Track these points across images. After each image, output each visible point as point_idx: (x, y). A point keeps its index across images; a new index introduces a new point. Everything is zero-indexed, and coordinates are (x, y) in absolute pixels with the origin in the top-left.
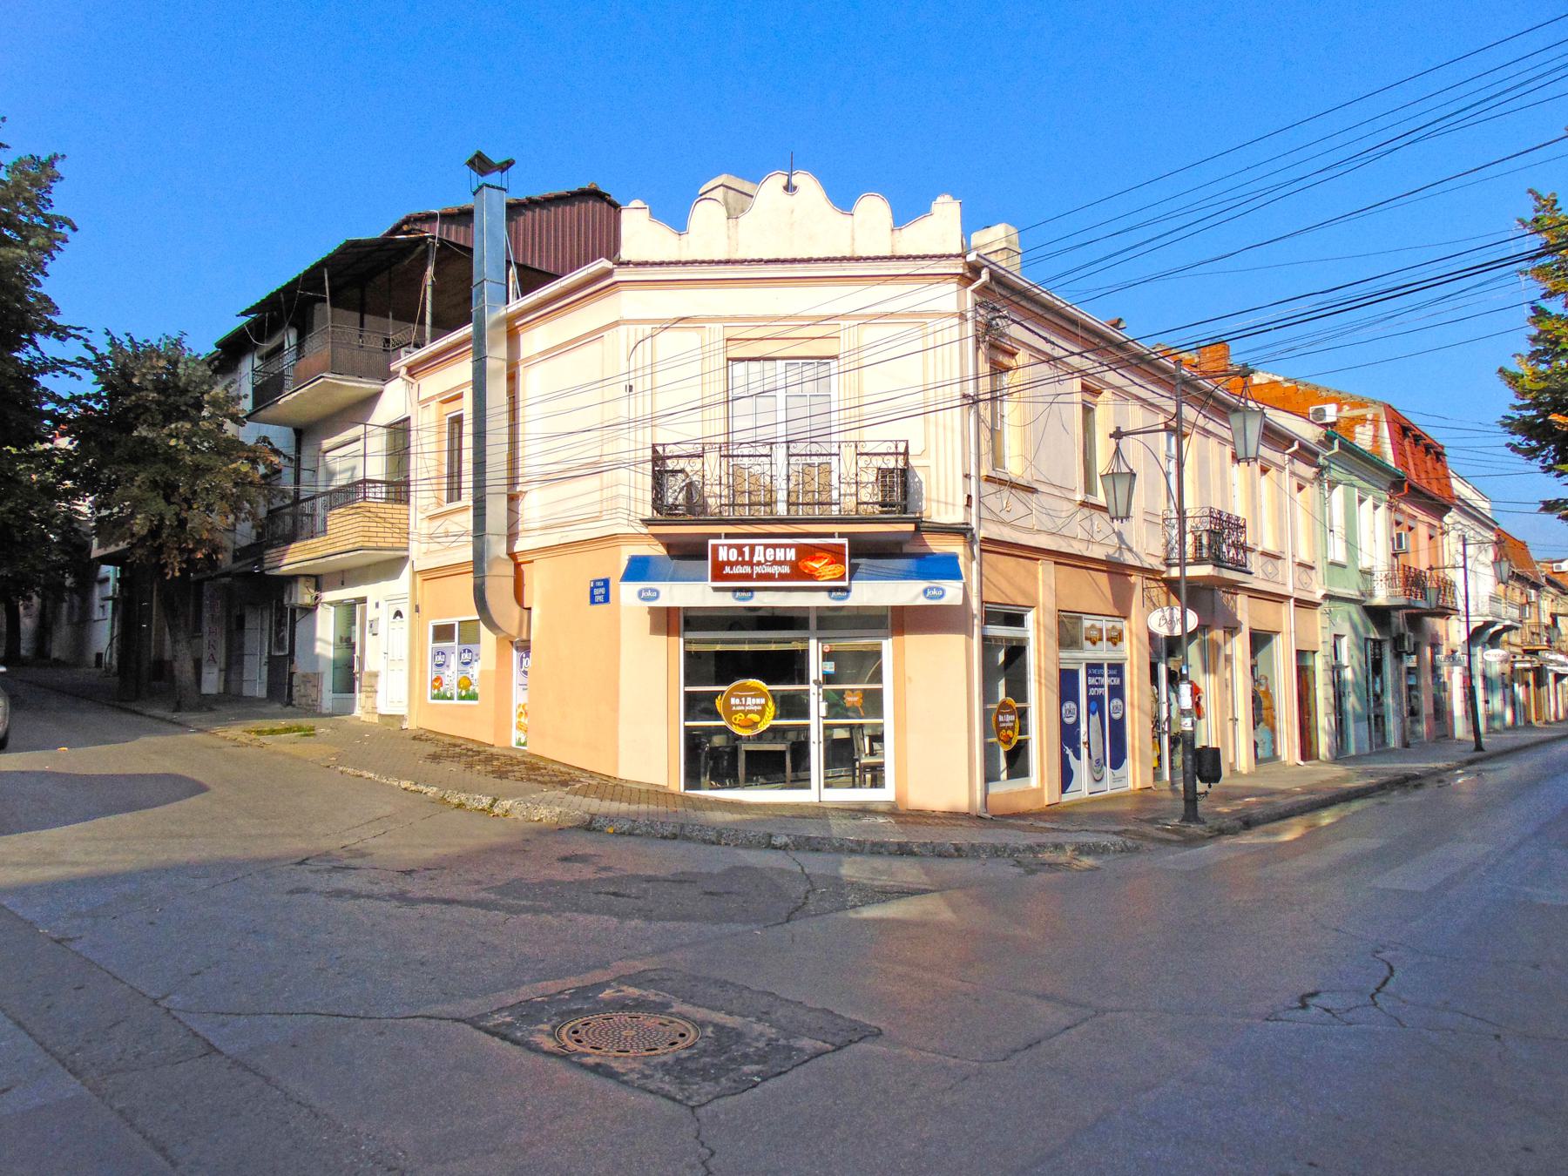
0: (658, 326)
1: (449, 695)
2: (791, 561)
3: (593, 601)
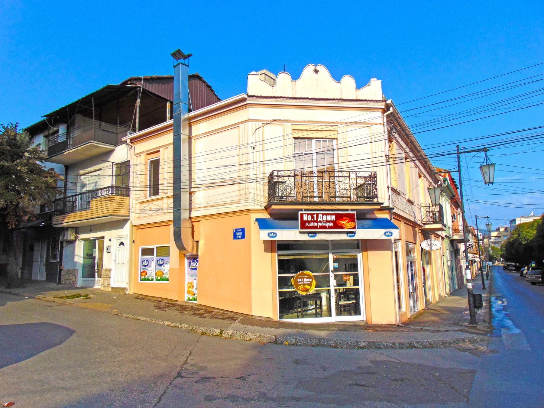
0: (265, 123)
1: (150, 279)
2: (333, 221)
3: (235, 237)
